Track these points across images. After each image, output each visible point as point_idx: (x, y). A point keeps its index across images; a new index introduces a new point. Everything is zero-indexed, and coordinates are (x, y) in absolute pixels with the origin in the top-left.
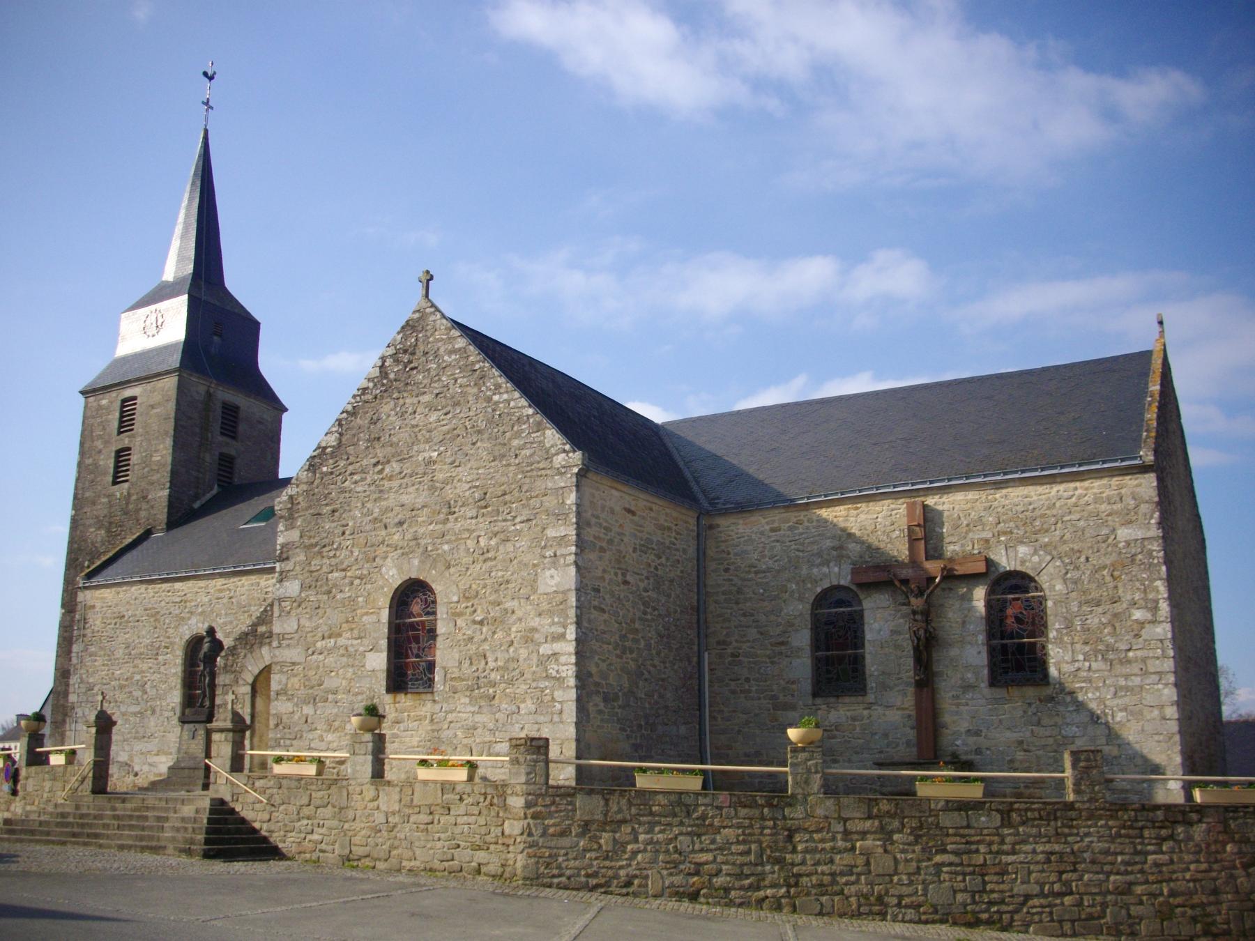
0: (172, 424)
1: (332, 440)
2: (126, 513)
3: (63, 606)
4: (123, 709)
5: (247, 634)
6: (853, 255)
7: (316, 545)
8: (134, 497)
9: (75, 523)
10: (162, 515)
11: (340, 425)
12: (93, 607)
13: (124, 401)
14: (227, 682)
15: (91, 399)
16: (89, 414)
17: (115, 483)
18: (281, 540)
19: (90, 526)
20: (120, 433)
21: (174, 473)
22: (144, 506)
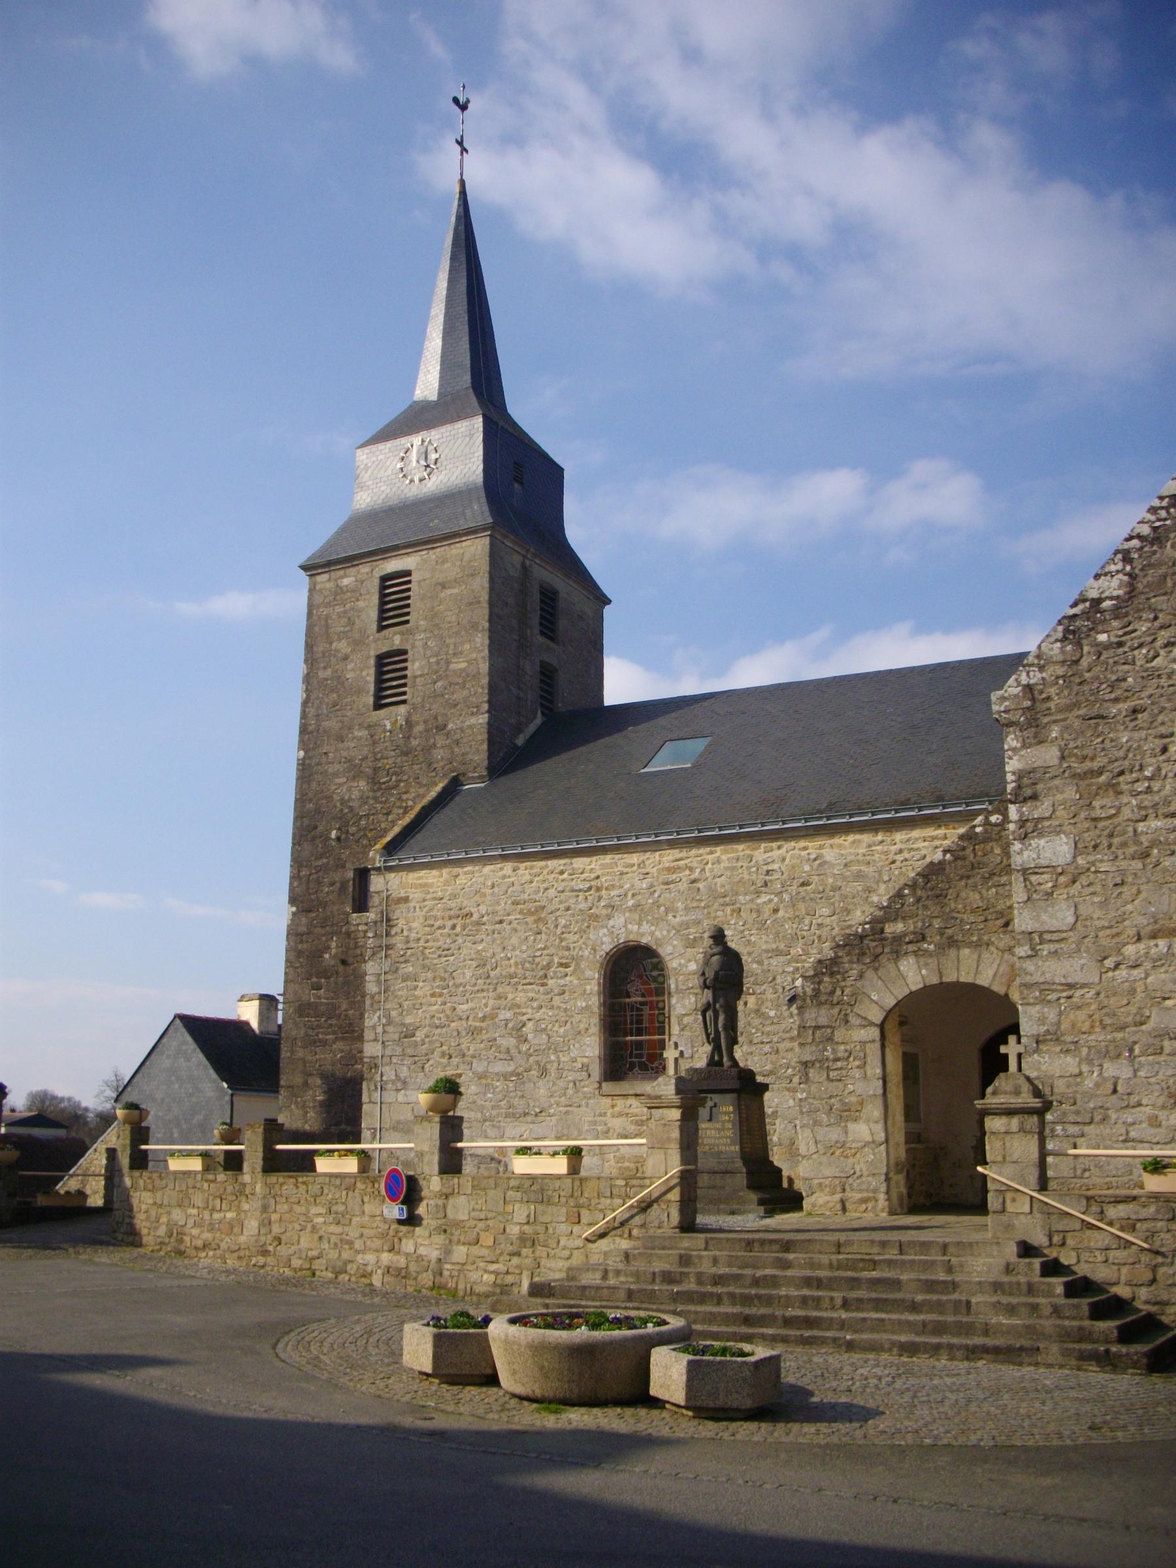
0: (486, 611)
1: (1113, 586)
2: (406, 754)
3: (293, 900)
4: (479, 1067)
5: (862, 937)
6: (883, 469)
7: (1100, 772)
8: (419, 728)
9: (306, 772)
10: (477, 753)
11: (1127, 559)
12: (406, 900)
13: (384, 579)
14: (823, 1021)
15: (319, 578)
16: (318, 599)
17: (378, 706)
18: (1012, 765)
19: (336, 774)
20: (381, 628)
21: (493, 689)
22: (441, 741)
